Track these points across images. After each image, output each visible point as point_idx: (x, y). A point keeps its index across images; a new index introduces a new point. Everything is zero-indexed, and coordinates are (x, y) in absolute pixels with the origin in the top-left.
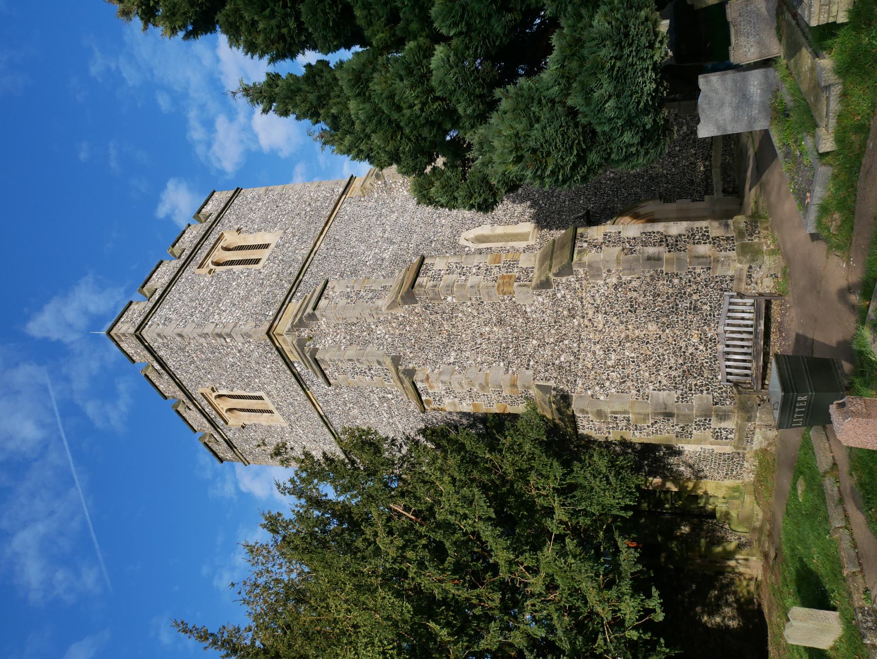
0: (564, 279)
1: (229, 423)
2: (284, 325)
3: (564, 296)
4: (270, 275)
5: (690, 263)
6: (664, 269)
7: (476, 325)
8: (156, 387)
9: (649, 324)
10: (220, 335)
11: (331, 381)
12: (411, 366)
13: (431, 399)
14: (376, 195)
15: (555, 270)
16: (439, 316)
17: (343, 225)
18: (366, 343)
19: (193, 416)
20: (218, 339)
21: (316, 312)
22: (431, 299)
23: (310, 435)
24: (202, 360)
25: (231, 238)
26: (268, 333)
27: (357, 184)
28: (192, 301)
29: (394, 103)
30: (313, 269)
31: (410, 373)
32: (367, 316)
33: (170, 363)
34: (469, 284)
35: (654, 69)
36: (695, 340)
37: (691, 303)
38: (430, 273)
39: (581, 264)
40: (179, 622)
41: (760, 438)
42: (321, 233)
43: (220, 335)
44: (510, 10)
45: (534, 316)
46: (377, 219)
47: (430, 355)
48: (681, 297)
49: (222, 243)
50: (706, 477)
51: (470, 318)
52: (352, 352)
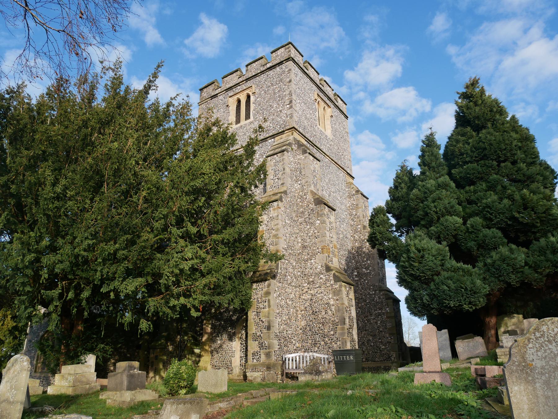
0: (332, 278)
1: (230, 98)
2: (296, 135)
3: (321, 278)
4: (314, 130)
5: (343, 339)
6: (339, 326)
7: (302, 235)
9: (305, 322)
10: (291, 102)
11: (269, 158)
12: (284, 200)
18: (291, 178)
19: (234, 79)
20: (289, 101)
21: (307, 154)
22: (318, 213)
24: (274, 90)
26: (294, 128)
27: (350, 180)
28: (304, 88)
29: (436, 200)
32: (306, 180)
33: (271, 73)
34: (326, 232)
35: (460, 305)
36: (297, 345)
37: (319, 341)
38: (329, 213)
39: (341, 286)
40: (163, 64)
41: (255, 375)
42: (332, 160)
44: (478, 249)
45: (309, 264)
46: (338, 189)
47: (288, 211)
48: (322, 336)
49: (326, 107)
50: (212, 356)
52: (288, 170)
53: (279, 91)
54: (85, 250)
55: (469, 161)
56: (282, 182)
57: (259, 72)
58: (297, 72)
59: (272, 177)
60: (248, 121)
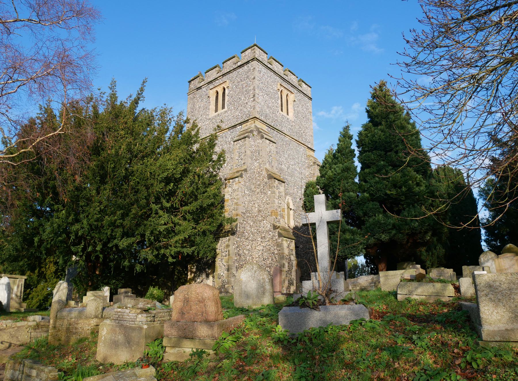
0: (277, 234)
3: (270, 234)
4: (276, 116)
8: (229, 60)
10: (254, 96)
12: (244, 176)
13: (230, 183)
14: (307, 161)
15: (280, 231)
16: (262, 188)
17: (295, 147)
18: (252, 158)
19: (213, 74)
22: (269, 185)
23: (205, 127)
24: (242, 85)
25: (291, 97)
26: (255, 117)
27: (311, 153)
30: (279, 135)
31: (241, 176)
33: (240, 70)
34: (275, 200)
38: (279, 185)
39: (282, 240)
42: (292, 138)
43: (254, 96)
49: (289, 93)
51: (261, 200)
52: (248, 152)
53: (246, 86)
54: (95, 221)
55: (367, 150)
56: (244, 162)
57: (232, 69)
58: (261, 69)
59: (237, 158)
60: (224, 110)
